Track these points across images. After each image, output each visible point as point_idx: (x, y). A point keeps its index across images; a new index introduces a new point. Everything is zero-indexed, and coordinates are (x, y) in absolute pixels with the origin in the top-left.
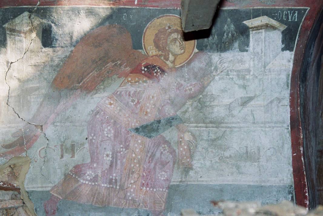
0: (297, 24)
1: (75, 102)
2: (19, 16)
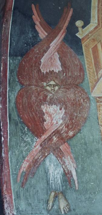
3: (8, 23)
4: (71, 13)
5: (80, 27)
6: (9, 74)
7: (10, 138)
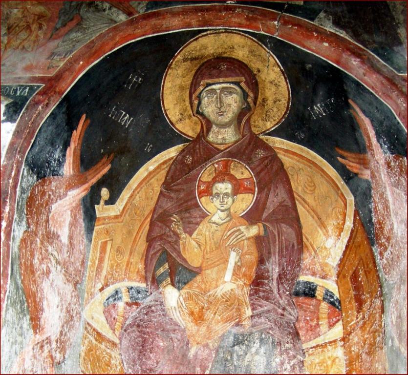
0: (26, 99)
1: (69, 363)
2: (192, 79)
3: (47, 111)
4: (106, 170)
5: (103, 200)
6: (398, 123)
7: (32, 138)
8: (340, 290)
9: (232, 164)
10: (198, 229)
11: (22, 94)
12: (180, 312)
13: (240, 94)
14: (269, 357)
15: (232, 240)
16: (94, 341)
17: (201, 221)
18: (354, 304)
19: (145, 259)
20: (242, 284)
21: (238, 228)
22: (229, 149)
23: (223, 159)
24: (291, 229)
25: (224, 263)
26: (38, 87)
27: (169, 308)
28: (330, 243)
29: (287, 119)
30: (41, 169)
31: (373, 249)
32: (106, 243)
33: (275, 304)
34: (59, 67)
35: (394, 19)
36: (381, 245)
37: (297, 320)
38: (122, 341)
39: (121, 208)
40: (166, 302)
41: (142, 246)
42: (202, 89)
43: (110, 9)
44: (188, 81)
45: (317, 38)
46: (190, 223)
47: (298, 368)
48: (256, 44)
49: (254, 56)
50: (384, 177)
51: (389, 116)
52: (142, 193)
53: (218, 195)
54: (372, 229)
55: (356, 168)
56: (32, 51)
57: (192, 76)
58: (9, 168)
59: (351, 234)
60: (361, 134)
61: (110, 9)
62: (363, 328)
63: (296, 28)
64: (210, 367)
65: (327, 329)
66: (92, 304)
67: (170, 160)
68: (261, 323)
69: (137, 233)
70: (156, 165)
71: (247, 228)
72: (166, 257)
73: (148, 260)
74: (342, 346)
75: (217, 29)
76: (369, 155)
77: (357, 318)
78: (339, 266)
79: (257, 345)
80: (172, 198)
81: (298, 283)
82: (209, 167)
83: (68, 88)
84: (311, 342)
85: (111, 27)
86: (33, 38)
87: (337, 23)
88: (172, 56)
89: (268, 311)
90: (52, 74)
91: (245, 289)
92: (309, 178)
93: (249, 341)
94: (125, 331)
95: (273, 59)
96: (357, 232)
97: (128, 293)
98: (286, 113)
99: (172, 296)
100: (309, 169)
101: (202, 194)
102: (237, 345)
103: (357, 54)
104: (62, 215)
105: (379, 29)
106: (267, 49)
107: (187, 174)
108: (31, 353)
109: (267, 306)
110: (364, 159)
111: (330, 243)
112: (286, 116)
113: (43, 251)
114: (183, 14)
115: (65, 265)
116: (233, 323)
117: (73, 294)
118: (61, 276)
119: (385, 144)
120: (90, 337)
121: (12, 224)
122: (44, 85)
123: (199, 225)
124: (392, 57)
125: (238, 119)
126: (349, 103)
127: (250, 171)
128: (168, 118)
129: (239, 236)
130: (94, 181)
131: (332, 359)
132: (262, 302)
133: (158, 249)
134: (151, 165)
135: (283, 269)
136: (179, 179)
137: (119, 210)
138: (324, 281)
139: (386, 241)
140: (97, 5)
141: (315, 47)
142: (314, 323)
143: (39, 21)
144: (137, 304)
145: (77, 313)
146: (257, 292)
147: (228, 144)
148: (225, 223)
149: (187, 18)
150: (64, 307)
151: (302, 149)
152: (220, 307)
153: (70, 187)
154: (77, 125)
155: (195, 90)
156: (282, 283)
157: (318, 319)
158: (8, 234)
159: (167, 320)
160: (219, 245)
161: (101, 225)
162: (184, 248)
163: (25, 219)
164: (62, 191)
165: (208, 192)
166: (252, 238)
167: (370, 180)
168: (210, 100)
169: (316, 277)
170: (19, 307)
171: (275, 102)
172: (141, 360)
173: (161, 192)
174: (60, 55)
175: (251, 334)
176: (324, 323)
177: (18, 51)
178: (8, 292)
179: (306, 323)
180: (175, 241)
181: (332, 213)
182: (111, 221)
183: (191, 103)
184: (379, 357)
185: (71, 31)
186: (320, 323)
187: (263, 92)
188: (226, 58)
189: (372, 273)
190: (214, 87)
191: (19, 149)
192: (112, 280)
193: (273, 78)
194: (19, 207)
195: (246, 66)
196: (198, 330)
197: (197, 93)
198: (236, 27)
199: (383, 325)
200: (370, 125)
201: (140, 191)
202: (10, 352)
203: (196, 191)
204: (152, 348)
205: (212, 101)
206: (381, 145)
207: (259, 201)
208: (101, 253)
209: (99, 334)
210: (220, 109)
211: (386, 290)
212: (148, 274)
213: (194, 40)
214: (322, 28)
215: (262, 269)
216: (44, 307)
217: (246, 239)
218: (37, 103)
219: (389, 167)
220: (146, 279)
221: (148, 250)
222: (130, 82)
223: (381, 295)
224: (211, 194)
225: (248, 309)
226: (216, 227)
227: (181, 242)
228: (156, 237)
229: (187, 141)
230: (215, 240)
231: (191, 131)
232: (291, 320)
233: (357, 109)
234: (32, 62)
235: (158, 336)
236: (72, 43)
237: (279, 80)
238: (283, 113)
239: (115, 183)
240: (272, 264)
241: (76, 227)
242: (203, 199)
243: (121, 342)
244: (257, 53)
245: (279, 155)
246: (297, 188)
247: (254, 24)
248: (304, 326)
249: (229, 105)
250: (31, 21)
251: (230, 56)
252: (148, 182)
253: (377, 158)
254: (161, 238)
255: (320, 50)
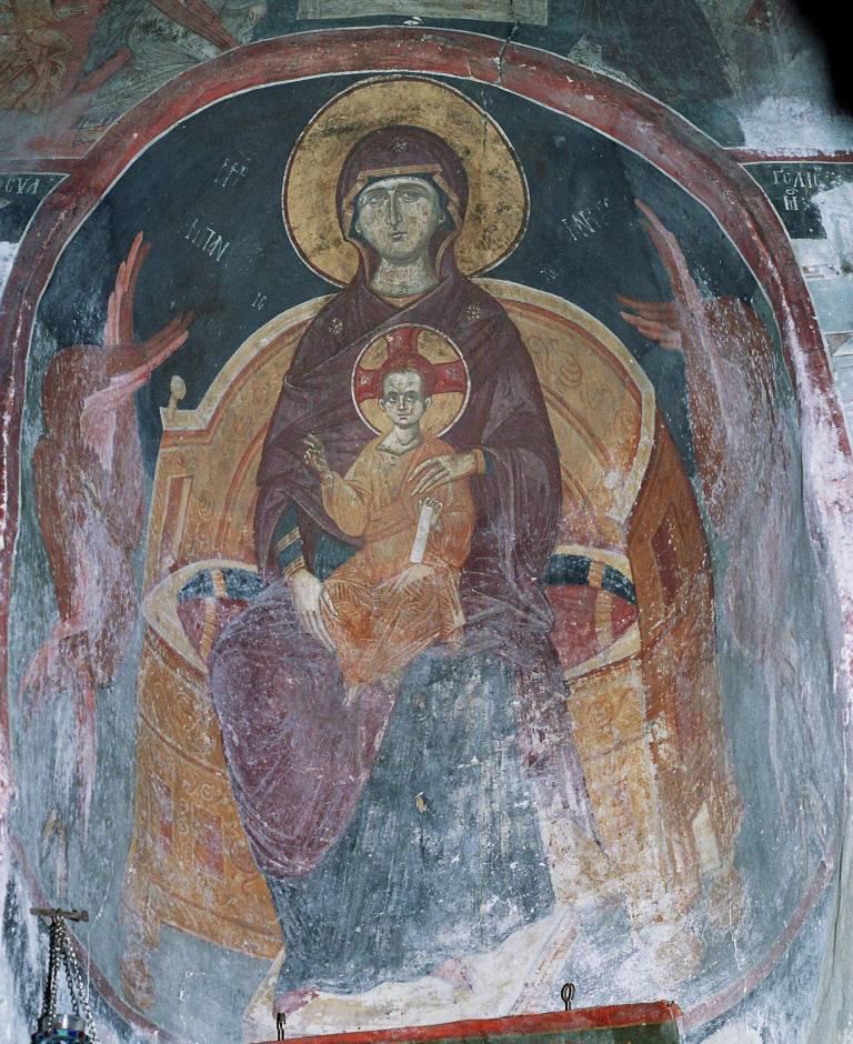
4: (180, 340)
6: (723, 236)
7: (49, 271)
8: (634, 566)
9: (421, 335)
10: (355, 464)
11: (28, 191)
12: (324, 622)
13: (432, 199)
14: (500, 699)
15: (424, 485)
16: (161, 663)
17: (362, 447)
18: (661, 589)
19: (255, 519)
20: (445, 566)
21: (435, 460)
22: (414, 306)
23: (402, 325)
24: (538, 459)
25: (408, 527)
26: (58, 178)
27: (304, 613)
28: (612, 480)
29: (524, 243)
30: (69, 331)
31: (693, 482)
32: (179, 482)
33: (509, 601)
34: (94, 144)
35: (717, 47)
36: (705, 472)
37: (553, 628)
38: (214, 670)
39: (209, 417)
40: (297, 601)
41: (248, 492)
42: (360, 188)
43: (185, 36)
44: (334, 172)
45: (573, 86)
46: (339, 451)
47: (556, 716)
48: (462, 101)
49: (459, 123)
50: (705, 342)
51: (708, 227)
52: (248, 391)
53: (394, 395)
54: (689, 444)
55: (656, 331)
56: (41, 111)
57: (342, 164)
58: (11, 321)
59: (652, 458)
60: (661, 264)
61: (185, 36)
62: (676, 631)
63: (534, 68)
64: (386, 724)
65: (611, 640)
66: (157, 592)
67: (300, 326)
68: (484, 639)
69: (239, 466)
70: (274, 336)
71: (453, 458)
72: (295, 515)
73: (260, 521)
74: (638, 668)
75: (387, 74)
76: (677, 302)
77: (666, 615)
78: (630, 520)
79: (477, 678)
80: (305, 400)
81: (555, 559)
82: (375, 341)
83: (111, 182)
84: (580, 666)
85: (188, 69)
86: (40, 89)
87: (610, 58)
88: (304, 126)
89: (498, 615)
90: (82, 154)
91: (450, 575)
92: (570, 358)
93: (461, 673)
94: (220, 651)
95: (493, 128)
96: (662, 451)
97: (223, 582)
98: (521, 231)
99: (308, 591)
100: (568, 340)
101: (364, 395)
102: (437, 681)
103: (648, 113)
104: (102, 419)
105: (690, 68)
106: (481, 110)
107: (333, 355)
108: (57, 653)
109: (496, 606)
110: (669, 311)
111: (612, 480)
112: (522, 237)
113: (72, 479)
114: (322, 47)
115: (107, 509)
116: (429, 640)
117: (124, 567)
118: (103, 531)
119: (703, 279)
120: (154, 653)
121: (19, 420)
122: (68, 175)
123: (358, 455)
124: (711, 118)
125: (431, 246)
126: (635, 206)
127: (457, 349)
128: (297, 244)
129: (437, 476)
130: (158, 360)
131: (621, 693)
132: (485, 600)
133: (279, 500)
134: (264, 336)
135: (524, 535)
136: (321, 373)
137: (204, 420)
138: (603, 551)
139: (715, 463)
140: (160, 29)
141: (570, 103)
142: (585, 632)
143: (50, 58)
144: (241, 603)
145: (130, 604)
146: (473, 581)
147: (413, 295)
148: (409, 450)
149: (331, 54)
150: (110, 586)
151: (554, 301)
152: (403, 611)
153: (115, 369)
154: (128, 251)
155: (348, 190)
156: (523, 562)
157: (593, 623)
158: (14, 437)
159: (300, 637)
160: (399, 494)
161: (171, 446)
162: (330, 499)
163: (40, 416)
164: (101, 374)
165: (374, 390)
166: (463, 477)
167: (682, 351)
168: (376, 210)
169: (587, 546)
170: (36, 565)
171: (500, 211)
172: (250, 708)
173: (284, 390)
174: (93, 121)
175: (465, 658)
176: (603, 630)
177: (14, 114)
178: (18, 534)
179: (569, 633)
180: (313, 486)
181: (614, 423)
182: (189, 440)
183: (340, 216)
184: (705, 677)
185: (111, 77)
186: (597, 630)
187: (476, 192)
188: (406, 127)
189: (691, 526)
190: (382, 184)
191: (26, 289)
192: (192, 554)
193: (494, 165)
194: (31, 393)
195: (443, 141)
196: (361, 656)
197: (351, 196)
198: (422, 69)
199: (713, 617)
200: (676, 245)
201: (243, 385)
202: (24, 638)
203: (352, 388)
204: (272, 687)
205: (380, 211)
206: (696, 281)
207: (474, 407)
208: (171, 499)
209: (170, 651)
210: (395, 227)
211: (716, 555)
212: (261, 547)
213: (344, 94)
214: (583, 68)
215: (483, 538)
216: (77, 575)
217: (452, 480)
218: (59, 207)
219: (712, 320)
220: (257, 559)
221: (260, 502)
222: (224, 174)
223: (709, 565)
224: (381, 396)
225: (457, 614)
226: (393, 458)
227: (323, 488)
228: (276, 476)
229: (330, 289)
230: (391, 483)
231: (340, 270)
232: (542, 629)
233: (652, 217)
234: (42, 133)
235: (283, 666)
236: (116, 99)
237: (505, 168)
238: (516, 232)
239: (197, 367)
240: (503, 528)
241: (126, 445)
242: (366, 404)
243: (211, 672)
244: (465, 117)
245: (510, 315)
246: (547, 378)
247: (457, 64)
248: (566, 638)
249: (413, 220)
250: (35, 58)
251: (413, 124)
252: (259, 368)
253: (690, 306)
254: (284, 477)
255: (580, 109)
